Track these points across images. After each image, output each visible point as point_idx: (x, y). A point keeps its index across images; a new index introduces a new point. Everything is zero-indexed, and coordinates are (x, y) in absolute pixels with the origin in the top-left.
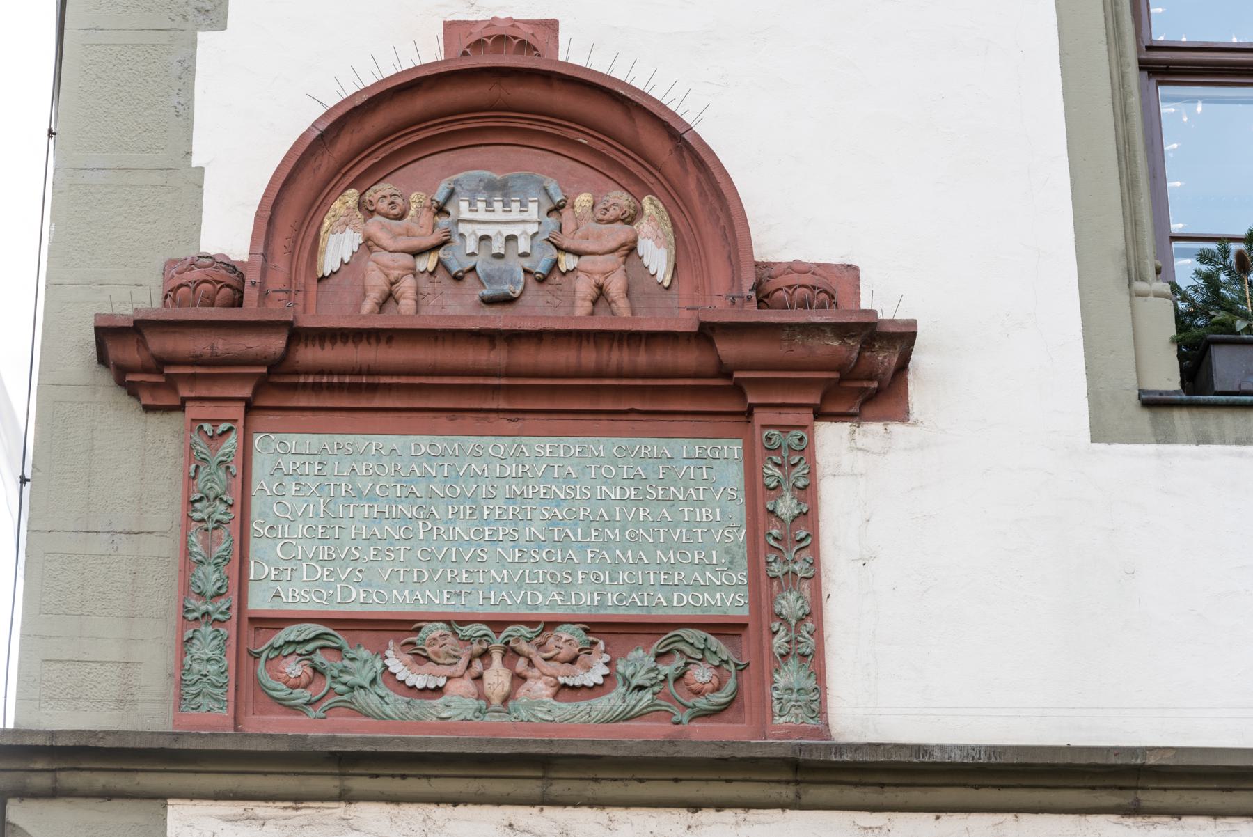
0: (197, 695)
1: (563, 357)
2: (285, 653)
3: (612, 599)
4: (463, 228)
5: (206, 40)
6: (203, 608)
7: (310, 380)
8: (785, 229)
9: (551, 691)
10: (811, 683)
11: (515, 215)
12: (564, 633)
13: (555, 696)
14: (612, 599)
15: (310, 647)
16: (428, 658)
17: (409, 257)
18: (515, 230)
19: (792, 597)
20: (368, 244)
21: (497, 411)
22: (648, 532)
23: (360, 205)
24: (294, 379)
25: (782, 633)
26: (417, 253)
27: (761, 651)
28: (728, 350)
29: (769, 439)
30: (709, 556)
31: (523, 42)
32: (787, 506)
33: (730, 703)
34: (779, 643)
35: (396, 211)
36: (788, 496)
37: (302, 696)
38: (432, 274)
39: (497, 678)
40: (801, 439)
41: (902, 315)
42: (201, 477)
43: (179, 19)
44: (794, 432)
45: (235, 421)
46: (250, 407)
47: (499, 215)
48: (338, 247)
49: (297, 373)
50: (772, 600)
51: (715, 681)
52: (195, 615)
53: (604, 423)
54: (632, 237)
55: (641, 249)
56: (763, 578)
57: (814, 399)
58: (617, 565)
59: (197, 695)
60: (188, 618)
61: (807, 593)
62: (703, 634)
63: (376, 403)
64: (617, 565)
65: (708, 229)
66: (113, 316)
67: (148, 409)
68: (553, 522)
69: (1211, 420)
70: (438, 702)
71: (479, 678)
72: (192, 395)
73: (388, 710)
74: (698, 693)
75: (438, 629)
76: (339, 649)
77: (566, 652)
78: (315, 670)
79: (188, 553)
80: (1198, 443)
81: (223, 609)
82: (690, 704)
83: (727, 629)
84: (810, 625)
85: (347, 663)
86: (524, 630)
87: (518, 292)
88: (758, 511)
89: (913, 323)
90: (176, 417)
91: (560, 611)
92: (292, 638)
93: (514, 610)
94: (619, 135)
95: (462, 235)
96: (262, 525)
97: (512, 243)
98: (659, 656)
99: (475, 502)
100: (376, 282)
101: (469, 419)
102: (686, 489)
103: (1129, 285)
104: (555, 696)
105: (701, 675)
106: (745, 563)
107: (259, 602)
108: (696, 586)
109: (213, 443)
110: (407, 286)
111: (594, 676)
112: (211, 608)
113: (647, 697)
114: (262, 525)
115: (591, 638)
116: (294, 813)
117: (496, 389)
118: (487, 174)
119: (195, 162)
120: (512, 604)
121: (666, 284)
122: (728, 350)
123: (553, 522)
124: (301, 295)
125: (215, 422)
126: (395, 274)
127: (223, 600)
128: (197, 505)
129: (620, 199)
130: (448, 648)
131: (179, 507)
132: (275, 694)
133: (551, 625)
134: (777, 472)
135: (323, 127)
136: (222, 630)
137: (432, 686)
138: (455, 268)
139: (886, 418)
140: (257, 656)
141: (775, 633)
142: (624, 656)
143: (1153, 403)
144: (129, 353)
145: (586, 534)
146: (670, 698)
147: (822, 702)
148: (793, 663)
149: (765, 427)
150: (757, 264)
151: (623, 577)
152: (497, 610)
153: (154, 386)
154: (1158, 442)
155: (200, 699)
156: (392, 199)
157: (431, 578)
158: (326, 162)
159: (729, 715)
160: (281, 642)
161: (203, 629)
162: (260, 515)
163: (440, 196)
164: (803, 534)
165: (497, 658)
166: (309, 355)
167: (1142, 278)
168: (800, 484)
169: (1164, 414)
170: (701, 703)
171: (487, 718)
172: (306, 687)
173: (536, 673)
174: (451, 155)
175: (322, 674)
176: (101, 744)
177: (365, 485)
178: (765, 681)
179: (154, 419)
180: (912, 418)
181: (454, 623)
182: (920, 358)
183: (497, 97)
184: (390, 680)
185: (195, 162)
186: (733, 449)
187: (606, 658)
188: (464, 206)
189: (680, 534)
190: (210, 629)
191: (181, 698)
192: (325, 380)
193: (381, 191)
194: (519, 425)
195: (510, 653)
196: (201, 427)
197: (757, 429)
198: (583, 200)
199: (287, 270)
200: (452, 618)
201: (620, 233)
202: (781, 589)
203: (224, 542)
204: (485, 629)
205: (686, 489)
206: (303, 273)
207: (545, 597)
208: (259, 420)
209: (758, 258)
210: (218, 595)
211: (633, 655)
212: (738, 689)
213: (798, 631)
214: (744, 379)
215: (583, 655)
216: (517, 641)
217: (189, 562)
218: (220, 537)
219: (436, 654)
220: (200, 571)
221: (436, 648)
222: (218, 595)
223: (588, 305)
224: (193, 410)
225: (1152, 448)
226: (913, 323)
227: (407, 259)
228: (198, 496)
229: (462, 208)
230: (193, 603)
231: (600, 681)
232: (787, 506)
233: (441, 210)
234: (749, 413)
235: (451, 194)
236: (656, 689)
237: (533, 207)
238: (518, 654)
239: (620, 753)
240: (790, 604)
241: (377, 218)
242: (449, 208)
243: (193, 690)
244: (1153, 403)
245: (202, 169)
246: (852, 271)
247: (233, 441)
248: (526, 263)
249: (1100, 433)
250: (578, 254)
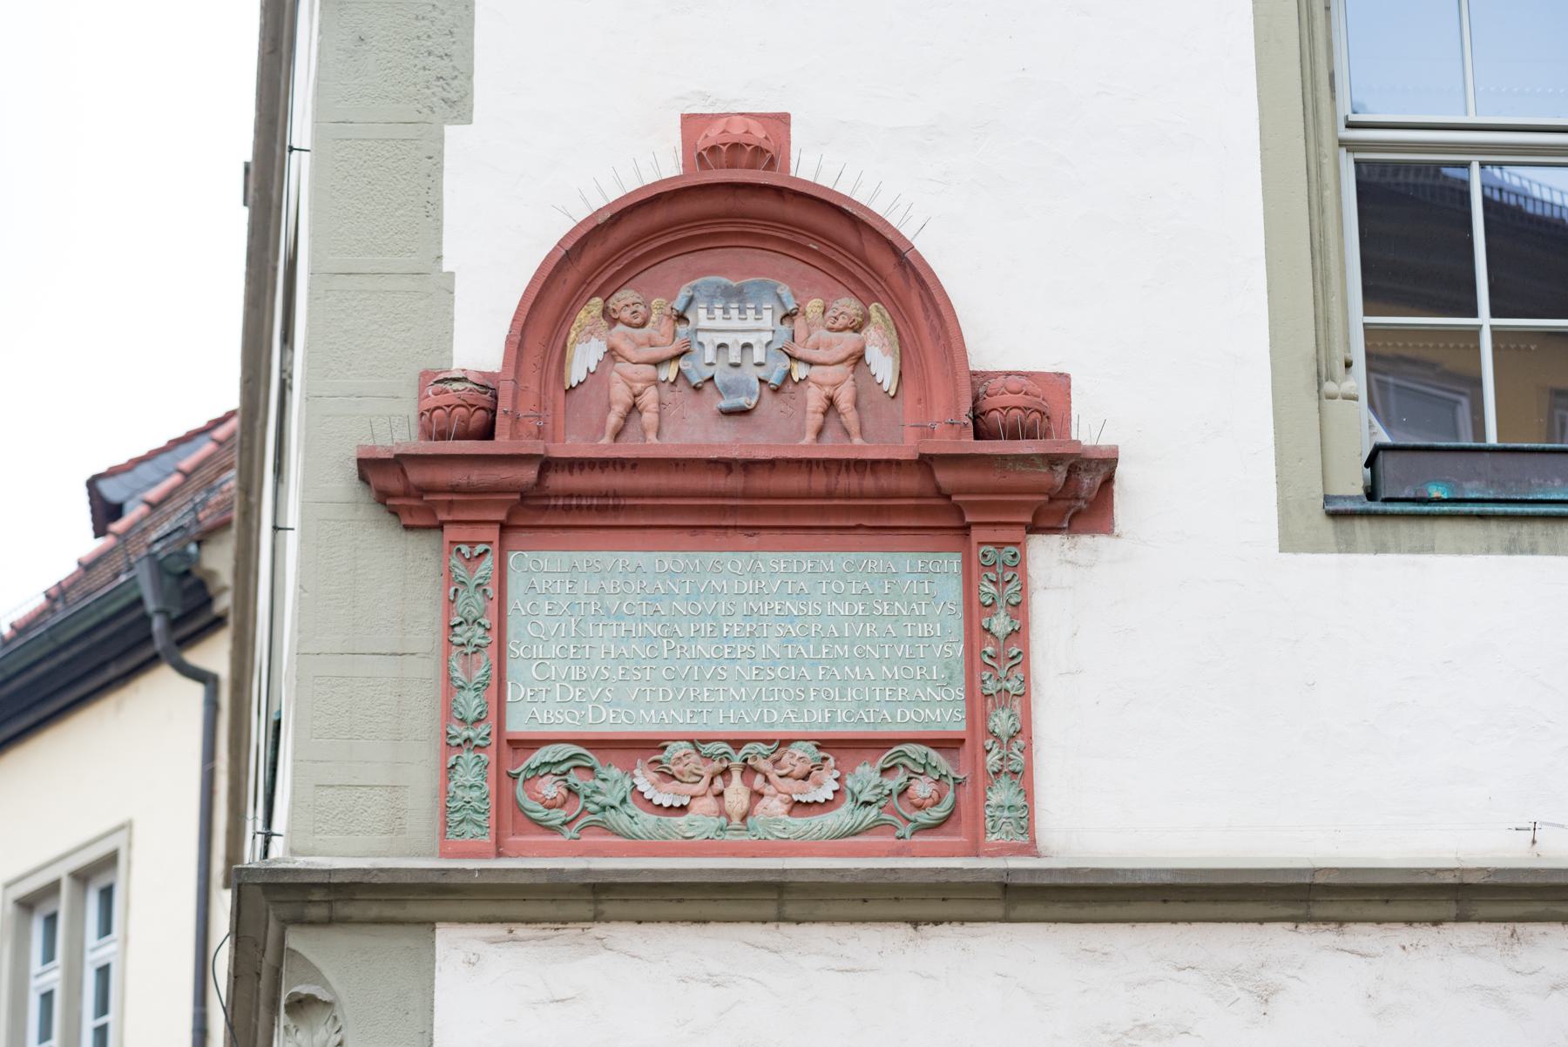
0: (461, 822)
1: (795, 482)
2: (541, 773)
3: (841, 716)
4: (701, 337)
5: (453, 134)
6: (465, 734)
7: (560, 502)
8: (1002, 333)
9: (786, 807)
10: (1020, 801)
11: (750, 323)
12: (797, 750)
13: (790, 813)
14: (841, 716)
15: (563, 768)
16: (673, 777)
17: (651, 368)
18: (750, 338)
19: (1004, 715)
20: (612, 354)
21: (735, 527)
22: (873, 646)
23: (605, 312)
24: (545, 502)
25: (995, 751)
26: (657, 364)
27: (975, 768)
28: (945, 478)
29: (985, 556)
30: (930, 672)
31: (757, 148)
32: (1000, 624)
33: (946, 819)
34: (992, 760)
35: (639, 320)
36: (1002, 613)
37: (558, 816)
38: (673, 384)
39: (737, 794)
40: (1014, 556)
41: (1105, 441)
42: (460, 600)
43: (426, 110)
44: (1008, 548)
45: (490, 543)
46: (504, 528)
47: (736, 323)
48: (584, 357)
49: (548, 497)
50: (986, 717)
51: (935, 795)
52: (458, 741)
53: (834, 538)
54: (859, 346)
55: (868, 358)
56: (978, 695)
57: (1028, 519)
58: (846, 682)
59: (461, 822)
60: (451, 745)
61: (1018, 710)
62: (924, 749)
63: (622, 521)
64: (846, 682)
65: (929, 345)
66: (374, 447)
67: (407, 528)
68: (787, 639)
69: (1388, 529)
70: (681, 821)
71: (720, 795)
72: (450, 518)
73: (635, 828)
74: (919, 807)
75: (682, 748)
76: (592, 769)
77: (800, 769)
78: (569, 790)
79: (450, 679)
80: (1376, 552)
81: (484, 734)
82: (912, 817)
83: (947, 744)
84: (1021, 742)
85: (599, 783)
86: (762, 748)
87: (753, 402)
88: (975, 632)
89: (1115, 450)
90: (435, 534)
91: (794, 729)
92: (547, 759)
93: (751, 728)
95: (701, 344)
96: (518, 646)
97: (748, 351)
98: (884, 771)
99: (715, 619)
100: (620, 395)
101: (709, 536)
102: (909, 604)
103: (1320, 384)
104: (790, 813)
105: (922, 788)
106: (963, 679)
107: (517, 725)
108: (917, 701)
109: (471, 564)
110: (649, 398)
111: (825, 793)
112: (472, 734)
113: (873, 812)
114: (518, 646)
115: (823, 754)
116: (553, 933)
117: (734, 510)
118: (724, 280)
119: (447, 266)
120: (750, 722)
121: (892, 393)
122: (945, 478)
123: (787, 639)
124: (550, 411)
125: (472, 544)
126: (639, 386)
127: (483, 725)
128: (457, 629)
129: (848, 306)
130: (691, 767)
131: (439, 627)
132: (533, 815)
133: (786, 743)
134: (992, 589)
135: (568, 246)
136: (483, 756)
137: (677, 804)
138: (696, 380)
139: (1092, 531)
140: (515, 777)
141: (988, 752)
142: (853, 771)
144: (393, 483)
145: (817, 651)
146: (895, 813)
147: (1031, 818)
148: (1004, 780)
149: (981, 544)
150: (975, 374)
151: (851, 693)
152: (735, 729)
153: (410, 509)
154: (1340, 552)
155: (464, 826)
156: (634, 308)
157: (675, 697)
158: (572, 276)
159: (947, 828)
160: (537, 763)
161: (465, 755)
162: (516, 636)
163: (679, 305)
164: (1015, 653)
165: (736, 775)
166: (559, 481)
167: (1330, 377)
168: (1013, 601)
169: (1346, 524)
170: (923, 817)
171: (728, 837)
172: (561, 807)
173: (768, 790)
174: (690, 257)
175: (576, 794)
176: (374, 881)
177: (613, 603)
178: (979, 800)
179: (412, 537)
180: (1116, 531)
181: (696, 742)
182: (1121, 470)
183: (733, 206)
184: (639, 798)
185: (447, 266)
186: (951, 562)
187: (837, 774)
188: (702, 313)
189: (903, 650)
190: (472, 755)
191: (446, 824)
192: (574, 502)
193: (625, 298)
194: (755, 539)
195: (748, 770)
196: (459, 550)
197: (974, 545)
198: (814, 306)
199: (536, 390)
200: (695, 738)
201: (849, 341)
202: (994, 706)
203: (482, 668)
204: (726, 747)
205: (909, 604)
206: (551, 386)
207: (780, 715)
208: (514, 538)
209: (975, 365)
210: (478, 721)
211: (860, 770)
212: (956, 802)
213: (1009, 748)
214: (966, 502)
215: (815, 772)
216: (755, 759)
217: (451, 686)
218: (479, 662)
219: (681, 773)
220: (461, 697)
221: (680, 767)
222: (478, 721)
223: (820, 417)
224: (451, 533)
225: (1334, 558)
226: (1115, 450)
227: (649, 370)
228: (457, 620)
229: (699, 316)
230: (456, 729)
231: (831, 797)
232: (1000, 624)
233: (681, 318)
234: (966, 529)
235: (691, 300)
236: (882, 803)
237: (767, 315)
238: (755, 771)
239: (848, 880)
240: (1002, 722)
241: (620, 327)
242: (689, 315)
243: (457, 817)
245: (452, 274)
246: (1060, 383)
247: (489, 562)
248: (761, 373)
249: (1290, 542)
250: (811, 364)
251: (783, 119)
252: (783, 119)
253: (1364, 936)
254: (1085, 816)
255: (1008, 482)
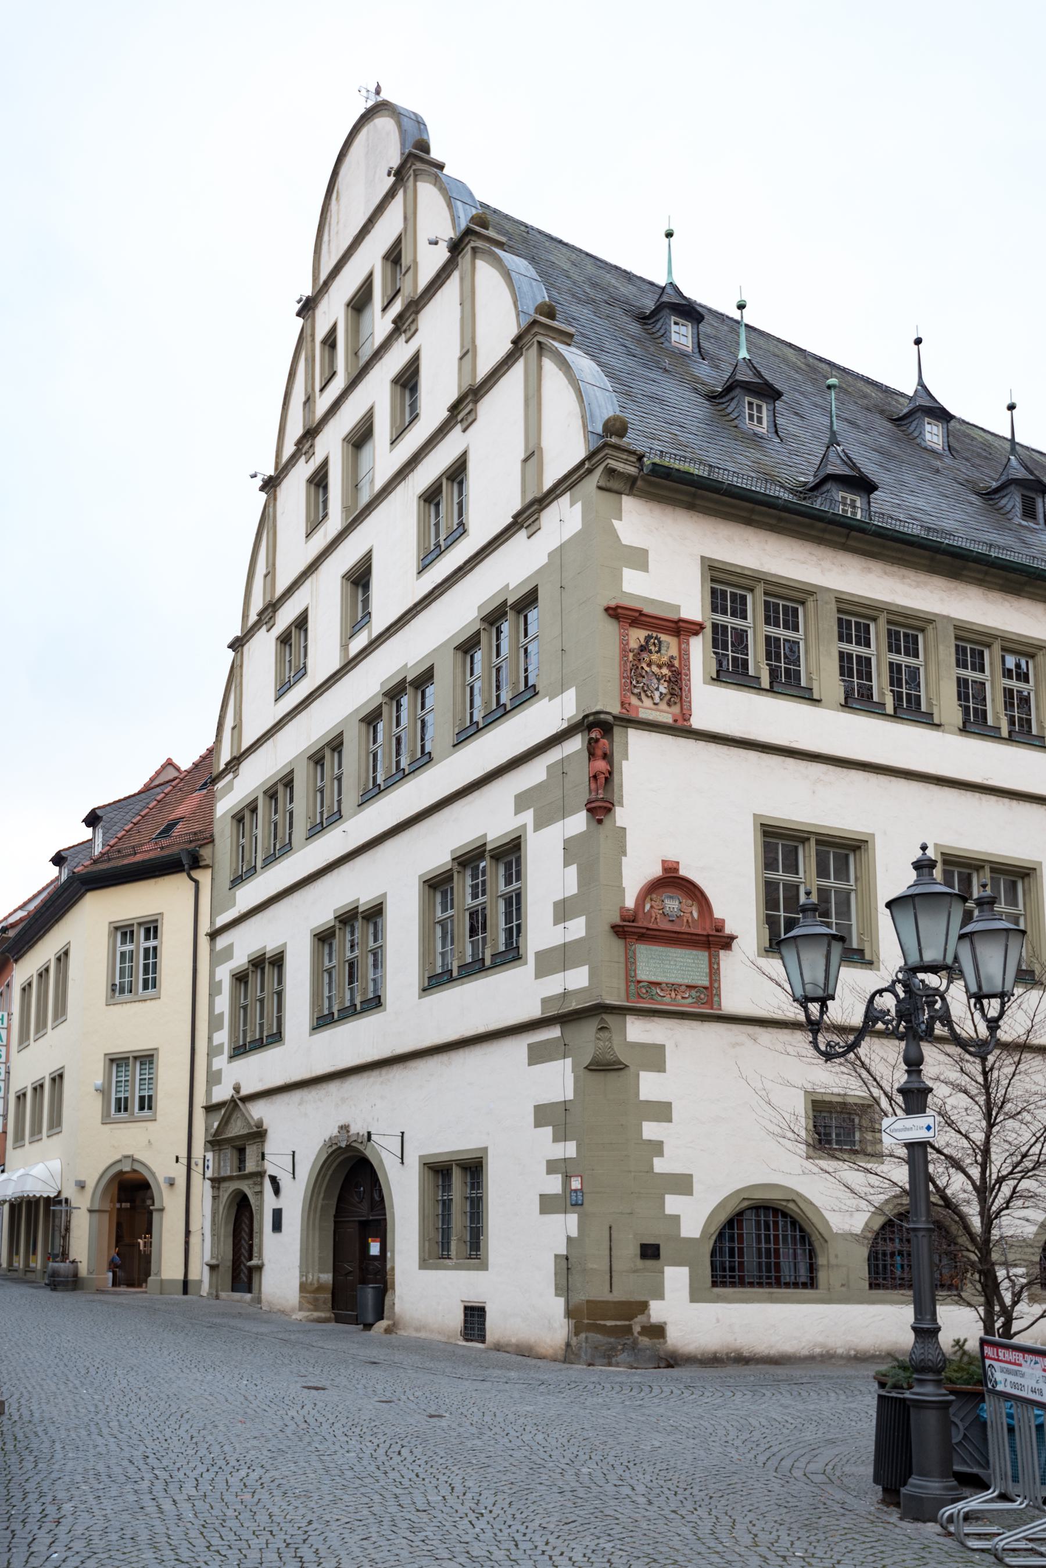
1: (686, 936)
20: (652, 907)
48: (647, 907)
83: (706, 988)
94: (692, 891)
107: (639, 978)
129: (690, 902)
143: (713, 679)
232: (716, 966)
244: (713, 679)
251: (678, 863)
252: (678, 863)
253: (770, 1030)
254: (731, 1002)
255: (716, 940)
